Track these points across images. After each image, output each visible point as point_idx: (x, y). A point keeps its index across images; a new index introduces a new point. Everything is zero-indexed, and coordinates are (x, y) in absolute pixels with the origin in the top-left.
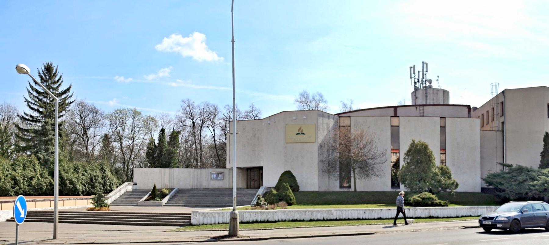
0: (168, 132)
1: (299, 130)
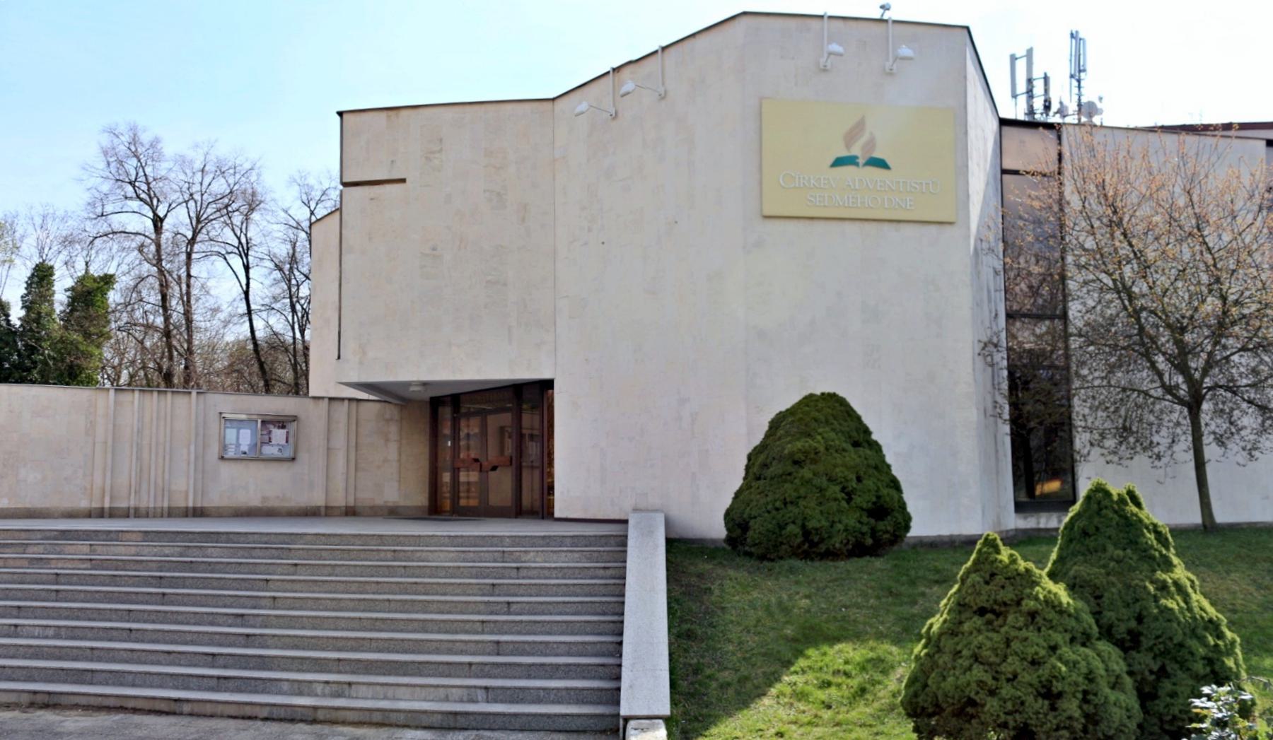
0: (62, 285)
1: (850, 138)
